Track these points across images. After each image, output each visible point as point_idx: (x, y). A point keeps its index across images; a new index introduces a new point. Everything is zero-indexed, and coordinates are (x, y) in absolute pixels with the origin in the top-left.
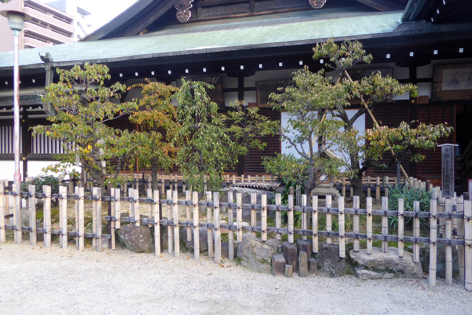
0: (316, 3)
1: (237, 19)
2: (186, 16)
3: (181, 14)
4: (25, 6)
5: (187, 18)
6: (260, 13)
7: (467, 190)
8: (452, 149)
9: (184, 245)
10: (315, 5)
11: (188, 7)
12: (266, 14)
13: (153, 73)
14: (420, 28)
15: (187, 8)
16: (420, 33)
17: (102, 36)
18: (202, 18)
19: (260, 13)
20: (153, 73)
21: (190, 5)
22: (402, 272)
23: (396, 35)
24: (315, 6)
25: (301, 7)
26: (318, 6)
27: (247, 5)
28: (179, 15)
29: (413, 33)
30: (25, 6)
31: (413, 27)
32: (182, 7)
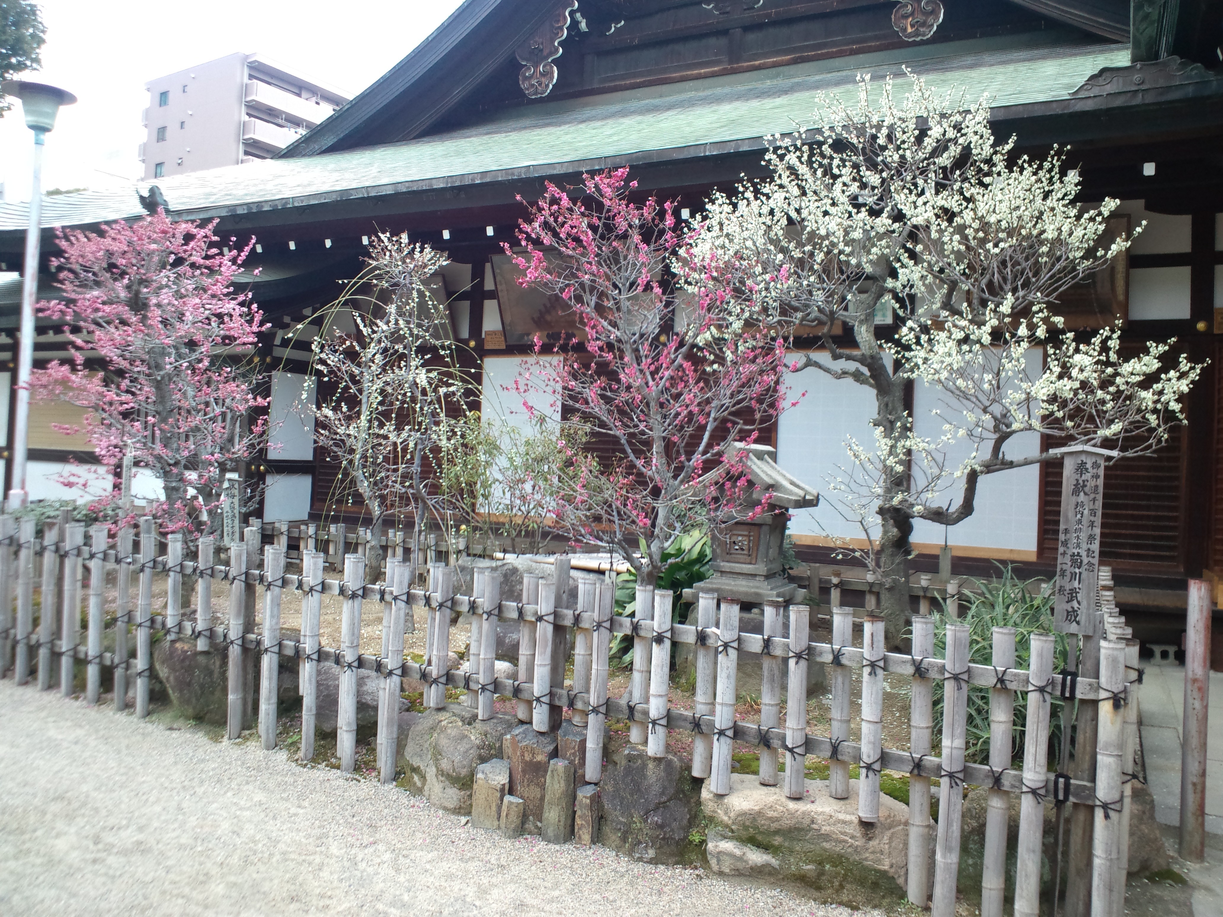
0: (912, 26)
1: (691, 84)
2: (544, 80)
3: (531, 77)
4: (251, 77)
5: (547, 86)
6: (757, 63)
7: (315, 449)
8: (1096, 465)
9: (861, 882)
10: (909, 30)
11: (551, 54)
12: (775, 65)
13: (446, 235)
14: (1162, 83)
15: (547, 57)
16: (1163, 99)
17: (330, 140)
18: (596, 86)
19: (757, 63)
20: (446, 235)
21: (557, 50)
22: (875, 886)
23: (1080, 107)
24: (909, 36)
25: (876, 38)
26: (917, 34)
27: (723, 41)
28: (526, 78)
29: (1138, 100)
30: (251, 77)
31: (1180, 78)
32: (537, 57)
